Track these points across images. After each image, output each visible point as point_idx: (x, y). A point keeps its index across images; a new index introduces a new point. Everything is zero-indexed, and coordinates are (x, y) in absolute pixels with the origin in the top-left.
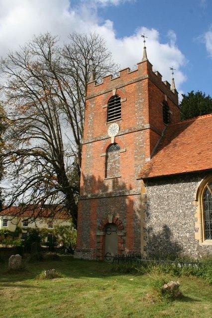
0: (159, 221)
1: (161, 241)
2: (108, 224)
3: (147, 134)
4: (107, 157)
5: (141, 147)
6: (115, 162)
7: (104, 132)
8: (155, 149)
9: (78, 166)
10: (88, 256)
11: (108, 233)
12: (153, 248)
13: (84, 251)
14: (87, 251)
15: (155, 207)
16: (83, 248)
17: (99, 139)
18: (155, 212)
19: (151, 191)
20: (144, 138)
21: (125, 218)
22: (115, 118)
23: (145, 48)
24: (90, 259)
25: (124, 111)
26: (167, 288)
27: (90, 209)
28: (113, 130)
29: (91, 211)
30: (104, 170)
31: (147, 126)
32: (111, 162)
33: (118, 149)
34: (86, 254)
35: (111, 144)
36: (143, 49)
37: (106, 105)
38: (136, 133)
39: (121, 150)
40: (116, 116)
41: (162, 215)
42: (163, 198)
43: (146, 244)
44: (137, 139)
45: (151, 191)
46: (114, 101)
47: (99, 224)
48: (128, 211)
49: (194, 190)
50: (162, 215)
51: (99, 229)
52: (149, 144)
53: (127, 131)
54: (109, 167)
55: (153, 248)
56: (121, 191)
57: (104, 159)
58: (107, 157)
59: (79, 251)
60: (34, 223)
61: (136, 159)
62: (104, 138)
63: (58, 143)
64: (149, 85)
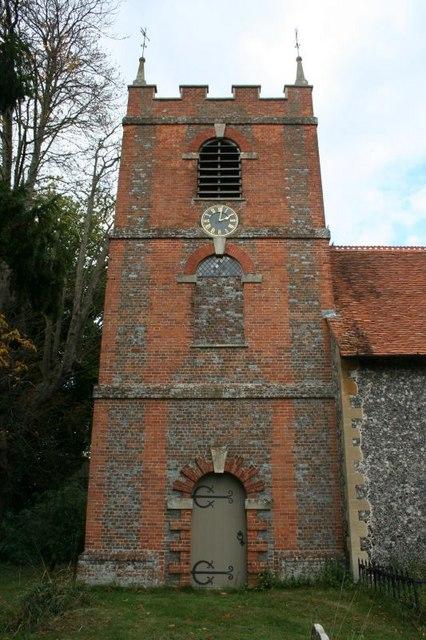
0: (400, 470)
1: (410, 521)
2: (211, 475)
5: (307, 279)
7: (188, 219)
10: (133, 577)
11: (202, 502)
12: (388, 541)
13: (118, 560)
14: (132, 561)
15: (385, 433)
16: (115, 551)
17: (171, 234)
18: (388, 446)
19: (372, 393)
21: (267, 460)
22: (219, 192)
23: (299, 59)
24: (145, 583)
25: (247, 182)
27: (141, 430)
34: (130, 568)
36: (296, 63)
37: (196, 155)
38: (292, 242)
40: (223, 188)
41: (406, 453)
42: (408, 412)
43: (366, 532)
44: (294, 259)
45: (372, 393)
46: (215, 157)
47: (174, 476)
48: (278, 442)
50: (406, 453)
51: (179, 490)
53: (265, 232)
55: (388, 541)
56: (250, 385)
59: (102, 562)
60: (92, 172)
61: (293, 307)
62: (191, 235)
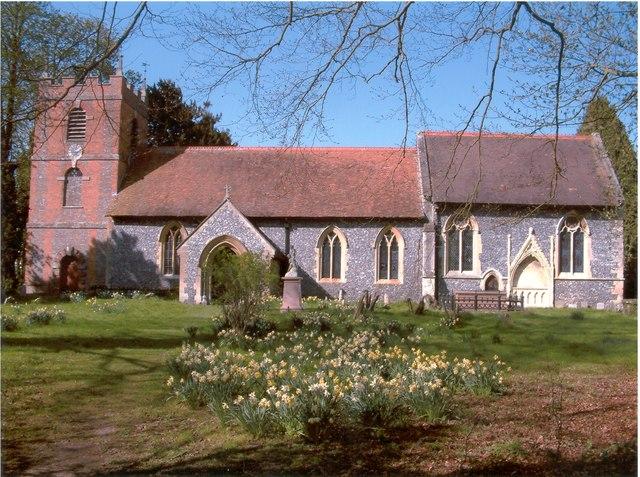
3: (115, 165)
4: (66, 182)
6: (75, 190)
8: (123, 184)
9: (85, 377)
20: (112, 169)
25: (88, 130)
26: (372, 455)
28: (75, 155)
29: (455, 372)
30: (62, 196)
31: (116, 156)
32: (70, 188)
33: (80, 174)
35: (72, 169)
39: (84, 178)
49: (254, 234)
52: (116, 176)
54: (68, 194)
57: (62, 184)
58: (66, 182)
63: (195, 466)
64: (122, 106)
